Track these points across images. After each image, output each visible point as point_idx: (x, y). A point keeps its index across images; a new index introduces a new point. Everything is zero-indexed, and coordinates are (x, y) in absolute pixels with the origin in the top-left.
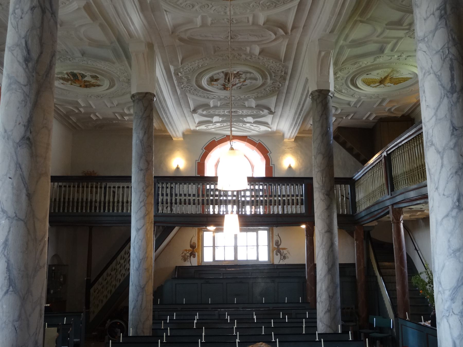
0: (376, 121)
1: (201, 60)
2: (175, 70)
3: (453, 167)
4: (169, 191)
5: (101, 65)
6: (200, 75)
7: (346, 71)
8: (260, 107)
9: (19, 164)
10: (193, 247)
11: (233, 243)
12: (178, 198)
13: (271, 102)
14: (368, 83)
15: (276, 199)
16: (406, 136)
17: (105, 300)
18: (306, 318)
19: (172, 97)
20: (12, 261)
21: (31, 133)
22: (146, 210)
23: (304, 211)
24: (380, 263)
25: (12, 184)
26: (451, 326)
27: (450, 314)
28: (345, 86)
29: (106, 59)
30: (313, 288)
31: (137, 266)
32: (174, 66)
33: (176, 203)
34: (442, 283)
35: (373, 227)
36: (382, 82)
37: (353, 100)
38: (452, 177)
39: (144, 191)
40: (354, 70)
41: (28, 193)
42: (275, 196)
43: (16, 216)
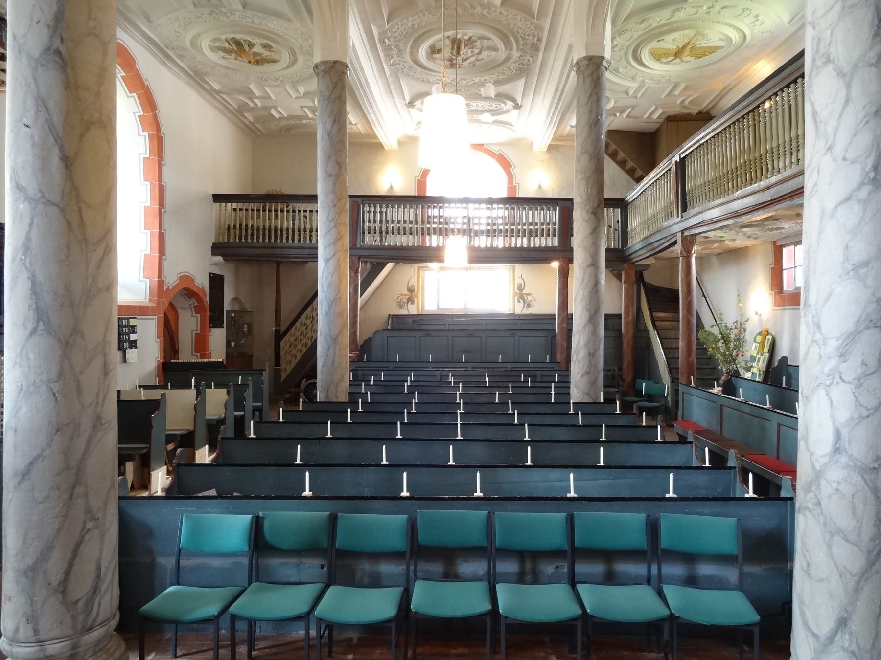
0: (661, 120)
1: (416, 17)
2: (380, 34)
3: (870, 101)
4: (378, 216)
5: (273, 25)
6: (417, 42)
7: (627, 35)
8: (501, 97)
9: (43, 100)
10: (411, 290)
11: (462, 287)
12: (390, 226)
13: (517, 88)
14: (658, 56)
15: (519, 227)
16: (714, 126)
17: (299, 356)
18: (555, 382)
19: (379, 82)
20: (40, 278)
21: (62, 40)
22: (338, 233)
23: (556, 244)
24: (654, 314)
25: (32, 137)
26: (834, 403)
27: (835, 382)
28: (623, 62)
29: (278, 15)
30: (565, 344)
31: (327, 310)
32: (378, 27)
33: (387, 233)
34: (823, 327)
35: (649, 265)
36: (678, 54)
37: (634, 85)
38: (867, 122)
39: (335, 206)
40: (640, 33)
41: (64, 156)
42: (519, 224)
43: (43, 196)
